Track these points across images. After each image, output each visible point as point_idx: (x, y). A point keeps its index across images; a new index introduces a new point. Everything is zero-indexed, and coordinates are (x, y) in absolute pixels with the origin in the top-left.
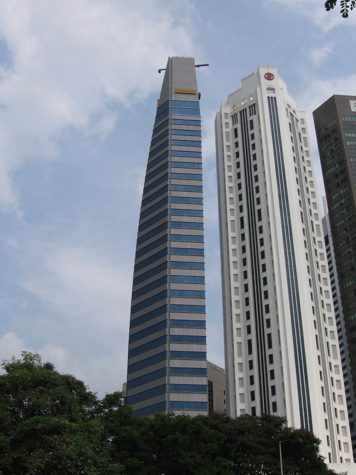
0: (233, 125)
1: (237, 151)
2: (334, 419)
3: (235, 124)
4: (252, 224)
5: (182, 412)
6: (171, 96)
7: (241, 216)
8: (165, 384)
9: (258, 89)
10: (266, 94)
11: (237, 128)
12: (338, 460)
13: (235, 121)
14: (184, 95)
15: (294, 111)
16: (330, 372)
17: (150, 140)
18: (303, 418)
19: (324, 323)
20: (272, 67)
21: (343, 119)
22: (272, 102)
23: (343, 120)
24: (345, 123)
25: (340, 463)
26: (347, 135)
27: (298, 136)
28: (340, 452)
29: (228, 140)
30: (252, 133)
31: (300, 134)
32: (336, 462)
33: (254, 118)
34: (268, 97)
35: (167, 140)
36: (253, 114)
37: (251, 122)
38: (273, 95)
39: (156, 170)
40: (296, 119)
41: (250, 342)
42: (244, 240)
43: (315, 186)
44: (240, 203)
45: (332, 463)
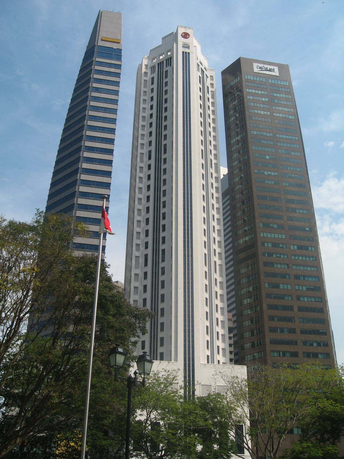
0: (151, 74)
1: (150, 121)
2: (215, 314)
3: (153, 73)
4: (156, 264)
5: (82, 252)
6: (97, 42)
7: (146, 229)
8: (71, 229)
9: (175, 45)
10: (181, 50)
11: (151, 151)
12: (216, 362)
13: (153, 72)
14: (109, 43)
15: (205, 69)
16: (215, 300)
17: (74, 87)
18: (186, 355)
19: (212, 211)
20: (189, 28)
21: (246, 76)
22: (186, 57)
23: (246, 78)
24: (248, 81)
25: (217, 364)
26: (248, 90)
27: (215, 336)
28: (218, 356)
29: (142, 161)
30: (164, 178)
31: (208, 87)
32: (214, 363)
33: (169, 68)
34: (183, 52)
35: (80, 145)
36: (168, 66)
37: (167, 72)
38: (187, 50)
39: (73, 114)
40: (206, 75)
41: (146, 256)
42: (151, 159)
43: (216, 131)
44: (149, 172)
45: (210, 363)
